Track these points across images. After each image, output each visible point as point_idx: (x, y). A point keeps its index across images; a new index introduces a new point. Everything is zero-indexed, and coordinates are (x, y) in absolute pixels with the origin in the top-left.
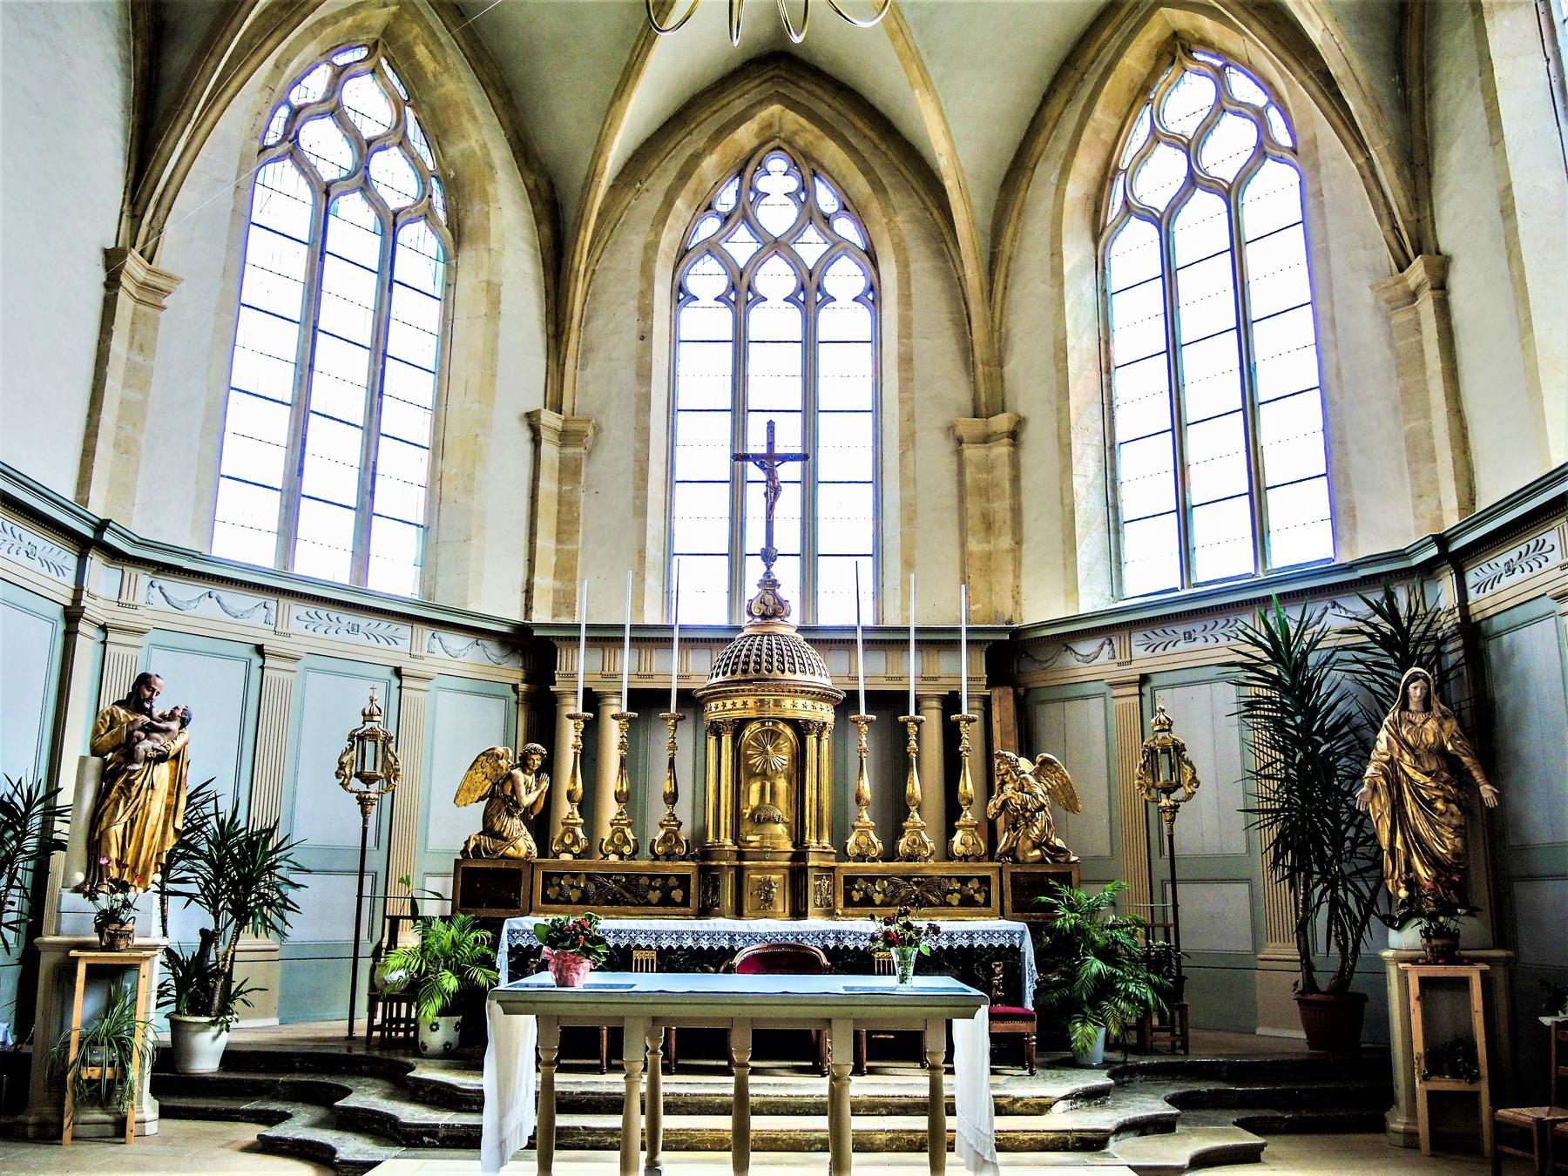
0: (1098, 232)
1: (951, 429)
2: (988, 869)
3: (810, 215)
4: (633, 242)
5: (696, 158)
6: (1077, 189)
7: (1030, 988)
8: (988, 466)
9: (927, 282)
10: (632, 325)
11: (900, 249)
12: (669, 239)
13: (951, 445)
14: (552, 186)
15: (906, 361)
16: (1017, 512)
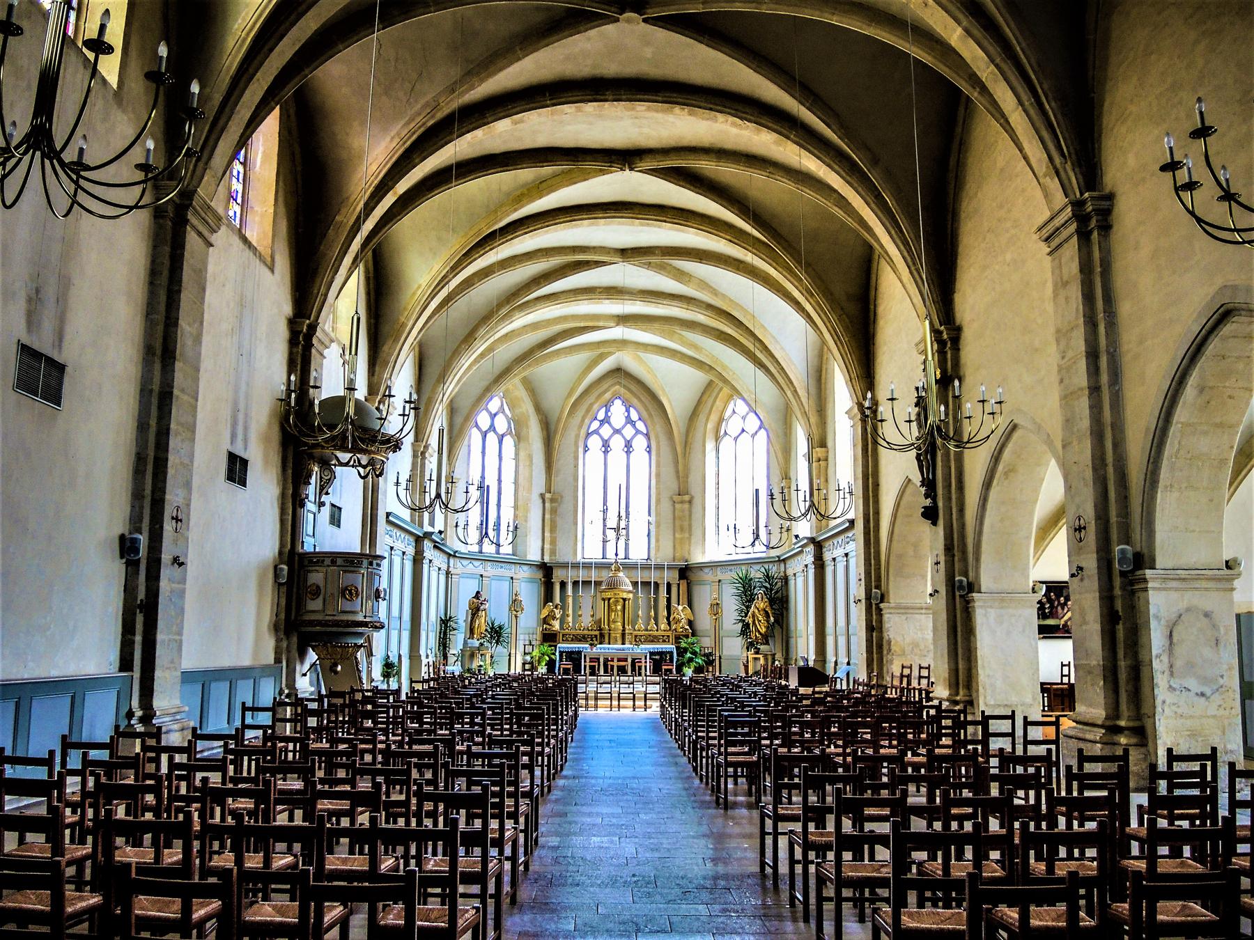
0: (717, 439)
1: (671, 498)
2: (669, 633)
3: (629, 421)
4: (571, 434)
5: (592, 404)
6: (710, 426)
7: (675, 660)
8: (683, 511)
9: (665, 449)
10: (572, 461)
11: (657, 437)
12: (583, 432)
13: (671, 503)
14: (546, 417)
15: (658, 475)
16: (690, 526)
